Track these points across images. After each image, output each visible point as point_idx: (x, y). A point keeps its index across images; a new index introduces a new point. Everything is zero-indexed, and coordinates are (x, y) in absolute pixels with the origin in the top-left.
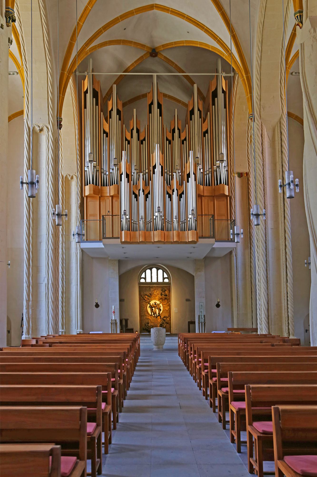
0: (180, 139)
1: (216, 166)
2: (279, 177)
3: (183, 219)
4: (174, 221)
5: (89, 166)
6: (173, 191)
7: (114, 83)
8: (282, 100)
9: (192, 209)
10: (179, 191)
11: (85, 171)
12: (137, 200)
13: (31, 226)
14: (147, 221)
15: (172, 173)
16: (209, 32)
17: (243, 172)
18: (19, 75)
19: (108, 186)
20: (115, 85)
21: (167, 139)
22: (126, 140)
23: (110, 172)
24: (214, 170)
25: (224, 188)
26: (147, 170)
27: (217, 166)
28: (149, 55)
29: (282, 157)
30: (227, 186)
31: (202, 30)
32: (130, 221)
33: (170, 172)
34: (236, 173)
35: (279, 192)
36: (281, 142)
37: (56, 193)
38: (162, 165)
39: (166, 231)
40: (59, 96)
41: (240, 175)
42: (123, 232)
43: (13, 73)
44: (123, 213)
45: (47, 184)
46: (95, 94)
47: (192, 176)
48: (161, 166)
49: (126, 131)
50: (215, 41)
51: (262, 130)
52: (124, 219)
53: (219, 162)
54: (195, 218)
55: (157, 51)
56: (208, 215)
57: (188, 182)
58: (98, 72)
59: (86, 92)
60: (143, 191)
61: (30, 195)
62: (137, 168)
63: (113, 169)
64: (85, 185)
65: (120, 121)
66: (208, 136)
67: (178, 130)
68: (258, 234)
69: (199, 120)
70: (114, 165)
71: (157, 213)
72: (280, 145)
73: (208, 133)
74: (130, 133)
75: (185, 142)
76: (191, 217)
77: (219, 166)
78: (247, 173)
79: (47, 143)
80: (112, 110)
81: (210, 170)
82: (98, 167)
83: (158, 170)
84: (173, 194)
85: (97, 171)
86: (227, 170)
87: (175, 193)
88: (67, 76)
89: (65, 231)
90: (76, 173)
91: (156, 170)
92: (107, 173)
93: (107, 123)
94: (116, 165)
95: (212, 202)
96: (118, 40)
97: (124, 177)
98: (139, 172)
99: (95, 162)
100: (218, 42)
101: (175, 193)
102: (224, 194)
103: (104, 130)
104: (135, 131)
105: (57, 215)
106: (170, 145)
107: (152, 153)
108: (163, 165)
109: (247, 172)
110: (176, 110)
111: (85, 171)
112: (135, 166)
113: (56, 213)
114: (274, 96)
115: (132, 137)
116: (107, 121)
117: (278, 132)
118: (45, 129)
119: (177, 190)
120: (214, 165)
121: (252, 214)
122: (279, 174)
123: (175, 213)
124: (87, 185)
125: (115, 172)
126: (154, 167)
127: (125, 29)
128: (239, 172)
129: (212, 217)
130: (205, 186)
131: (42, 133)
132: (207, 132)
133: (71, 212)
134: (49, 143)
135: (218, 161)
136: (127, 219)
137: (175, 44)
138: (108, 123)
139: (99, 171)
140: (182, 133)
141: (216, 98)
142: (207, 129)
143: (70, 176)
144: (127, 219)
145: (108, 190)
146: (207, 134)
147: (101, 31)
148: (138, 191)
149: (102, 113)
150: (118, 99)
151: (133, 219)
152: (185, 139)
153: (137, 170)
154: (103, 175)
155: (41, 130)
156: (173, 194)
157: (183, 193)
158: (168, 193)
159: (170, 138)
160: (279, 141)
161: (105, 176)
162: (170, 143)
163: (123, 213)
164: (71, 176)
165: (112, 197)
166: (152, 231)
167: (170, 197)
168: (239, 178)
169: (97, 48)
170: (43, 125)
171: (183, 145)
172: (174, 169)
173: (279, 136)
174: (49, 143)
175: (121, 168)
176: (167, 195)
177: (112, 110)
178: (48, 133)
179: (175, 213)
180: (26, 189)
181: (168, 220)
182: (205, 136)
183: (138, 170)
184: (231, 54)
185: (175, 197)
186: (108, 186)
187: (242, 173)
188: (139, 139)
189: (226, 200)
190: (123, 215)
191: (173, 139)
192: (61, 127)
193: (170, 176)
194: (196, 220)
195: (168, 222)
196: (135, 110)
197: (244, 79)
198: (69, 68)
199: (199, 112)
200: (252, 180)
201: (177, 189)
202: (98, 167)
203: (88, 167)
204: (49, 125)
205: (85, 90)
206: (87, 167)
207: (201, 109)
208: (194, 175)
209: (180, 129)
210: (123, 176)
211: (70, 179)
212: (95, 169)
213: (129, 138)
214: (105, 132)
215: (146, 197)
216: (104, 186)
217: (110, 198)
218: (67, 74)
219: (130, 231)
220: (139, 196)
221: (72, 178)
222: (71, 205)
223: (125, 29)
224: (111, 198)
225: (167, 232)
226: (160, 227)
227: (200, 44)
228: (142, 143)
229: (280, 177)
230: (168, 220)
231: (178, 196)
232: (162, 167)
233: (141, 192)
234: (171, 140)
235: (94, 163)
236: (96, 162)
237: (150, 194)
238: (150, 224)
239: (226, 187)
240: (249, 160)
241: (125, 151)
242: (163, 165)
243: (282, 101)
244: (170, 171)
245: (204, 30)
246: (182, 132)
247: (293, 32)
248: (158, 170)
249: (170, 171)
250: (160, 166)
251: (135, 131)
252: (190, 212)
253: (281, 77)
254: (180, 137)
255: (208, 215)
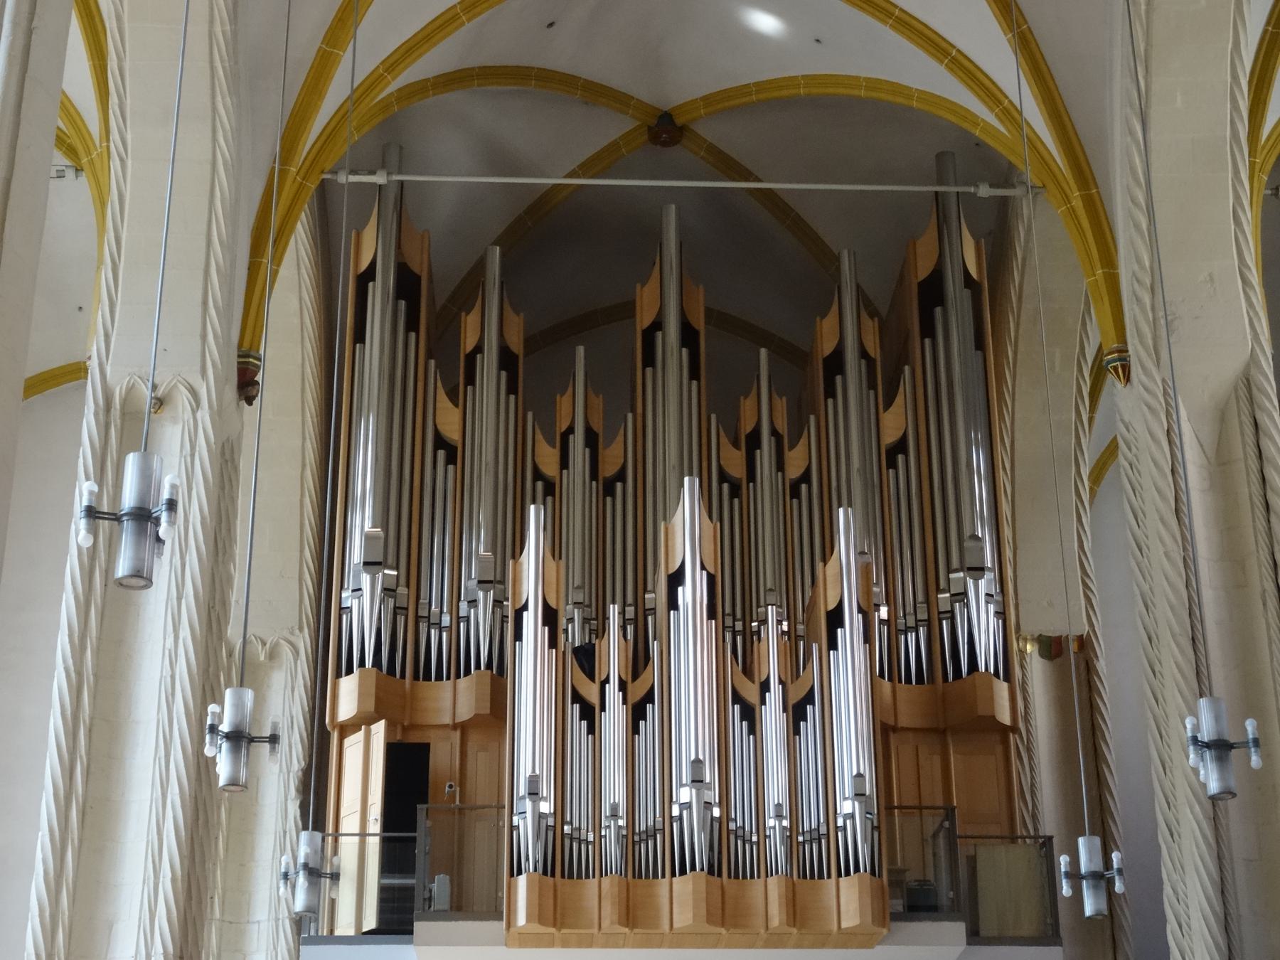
0: (780, 474)
1: (948, 595)
2: (1263, 621)
3: (811, 819)
4: (770, 828)
5: (360, 589)
6: (765, 687)
7: (495, 243)
8: (1248, 290)
9: (855, 772)
10: (790, 687)
11: (341, 609)
12: (591, 730)
13: (73, 840)
14: (637, 831)
15: (747, 624)
16: (913, 28)
17: (1064, 636)
18: (83, 178)
19: (448, 678)
20: (498, 248)
21: (723, 477)
22: (538, 475)
23: (459, 618)
24: (940, 613)
25: (990, 688)
26: (633, 608)
27: (952, 595)
28: (646, 137)
29: (1270, 529)
30: (1005, 685)
31: (885, 23)
32: (555, 827)
33: (739, 620)
34: (1033, 640)
35: (1064, 892)
36: (1259, 468)
37: (208, 688)
38: (712, 571)
39: (729, 876)
40: (281, 171)
41: (1052, 648)
42: (522, 881)
43: (57, 171)
44: (522, 789)
45: (170, 641)
46: (407, 285)
47: (854, 624)
48: (709, 575)
49: (539, 437)
50: (942, 62)
51: (1168, 414)
52: (529, 815)
53: (961, 574)
54: (868, 816)
55: (679, 121)
56: (927, 808)
57: (833, 645)
58: (435, 175)
59: (367, 277)
60: (623, 686)
61: (126, 574)
62: (584, 600)
63: (473, 603)
64: (338, 675)
65: (512, 397)
66: (909, 464)
67: (773, 438)
68: (1181, 893)
69: (868, 395)
70: (480, 582)
71: (688, 788)
72: (1255, 478)
73: (906, 452)
74: (554, 447)
75: (804, 487)
76: (850, 811)
77: (965, 594)
78: (1080, 638)
79: (185, 457)
80: (479, 349)
81: (923, 615)
82: (402, 590)
83: (692, 594)
84: (765, 704)
85: (398, 611)
86: (1002, 611)
87: (774, 696)
88: (296, 185)
89: (223, 902)
90: (292, 633)
91: (685, 594)
92: (446, 620)
93: (452, 406)
94: (490, 585)
95: (937, 760)
96: (518, 69)
97: (530, 620)
98: (594, 616)
99: (391, 568)
100: (951, 65)
101: (774, 696)
102: (994, 717)
103: (437, 435)
104: (578, 440)
105: (228, 736)
106: (736, 501)
107: (665, 519)
108: (716, 570)
109: (1080, 634)
110: (763, 352)
111: (341, 609)
112: (578, 588)
113: (225, 727)
114: (1211, 275)
115: (564, 463)
116: (453, 396)
117: (1241, 423)
118: (183, 398)
119: (781, 682)
120: (938, 590)
121: (1195, 740)
122: (1265, 604)
123: (776, 790)
124: (350, 671)
125: (481, 617)
126: (676, 579)
127: (551, 25)
128: (1044, 634)
129: (947, 815)
130: (900, 681)
131: (166, 413)
132: (900, 446)
133: (255, 815)
134: (192, 456)
135: (956, 571)
136: (540, 817)
137: (758, 92)
138: (457, 405)
139: (407, 609)
140: (790, 450)
141: (938, 306)
142: (901, 433)
143: (264, 644)
144: (540, 817)
145: (448, 695)
146: (900, 458)
147: (455, 18)
148: (595, 688)
149: (432, 362)
150: (507, 306)
151: (568, 819)
152: (806, 477)
153: (587, 606)
154: (423, 627)
155: (160, 403)
156: (763, 702)
157: (809, 698)
158: (737, 698)
159: (737, 469)
160: (1250, 462)
161: (434, 633)
162: (735, 491)
163: (522, 789)
164: (268, 645)
165: (463, 728)
166: (663, 876)
167: (750, 716)
168: (1042, 660)
169: (431, 92)
170: (173, 379)
171: (795, 501)
172: (758, 606)
173: (1250, 439)
174: (192, 456)
175: (521, 580)
176: (737, 707)
177: (479, 349)
178: (194, 412)
179: (776, 790)
180: (64, 661)
181: (739, 823)
182: (892, 464)
183: (590, 606)
184: (1011, 114)
185: (773, 716)
186: (448, 678)
187: (1061, 636)
188: (594, 475)
189: (999, 749)
190: (523, 798)
191: (751, 476)
192: (254, 393)
193: (739, 639)
194: (875, 824)
195: (740, 833)
196: (581, 351)
197: (1072, 212)
198: (308, 153)
199: (863, 362)
200: (1105, 671)
201: (783, 679)
202: (402, 590)
203: (360, 592)
204: (200, 377)
205: (364, 264)
206: (353, 591)
207: (873, 349)
208: (860, 616)
209: (780, 432)
210: (528, 618)
211: (262, 658)
212: (391, 602)
213: (550, 466)
214: (440, 442)
215: (637, 714)
216: (427, 677)
217: (452, 733)
218: (298, 178)
219: (553, 875)
220: (603, 708)
221: (273, 655)
222: (258, 779)
223: (551, 25)
224: (457, 735)
225: (736, 881)
226: (701, 858)
227: (867, 89)
228: (609, 490)
229: (1267, 620)
230: (739, 823)
231: (785, 710)
232: (711, 579)
233: (612, 691)
234: (741, 479)
235: (387, 572)
236: (397, 568)
237: (653, 704)
238: (651, 843)
239: (1002, 688)
240: (1088, 581)
241: (542, 507)
242: (716, 570)
243: (1251, 294)
244: (739, 614)
245: (891, 21)
246: (792, 447)
247: (1270, 29)
248: (692, 594)
249: (739, 614)
250: (705, 572)
251: (578, 440)
252: (845, 785)
253: (1237, 197)
254: (780, 466)
255: (927, 808)
